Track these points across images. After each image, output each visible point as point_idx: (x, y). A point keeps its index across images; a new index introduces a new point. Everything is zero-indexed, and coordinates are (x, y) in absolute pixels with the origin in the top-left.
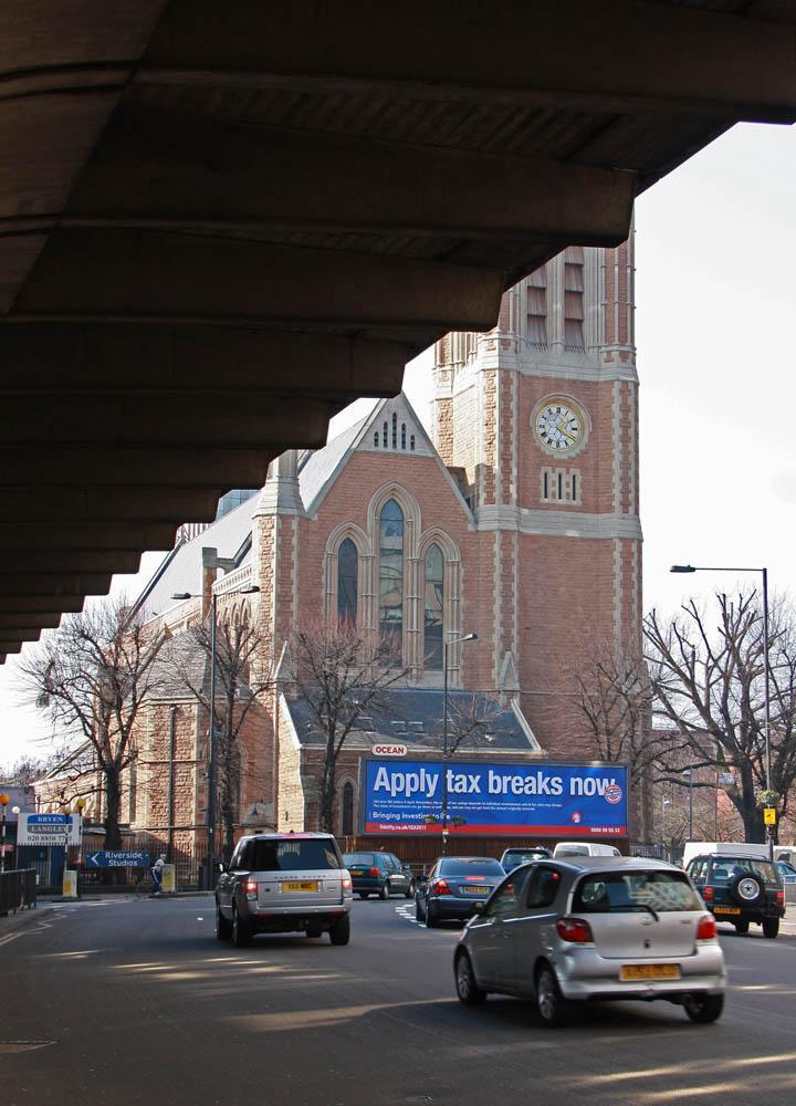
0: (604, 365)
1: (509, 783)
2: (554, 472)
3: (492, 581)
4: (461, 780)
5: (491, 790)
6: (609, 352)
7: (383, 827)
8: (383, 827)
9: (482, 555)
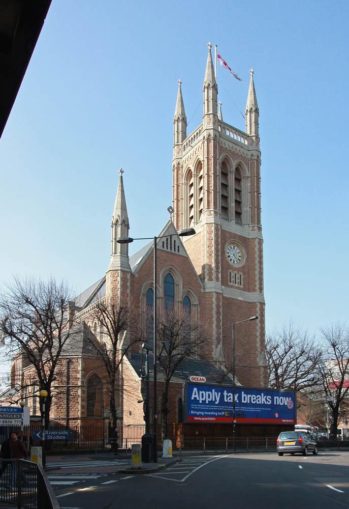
0: (251, 232)
1: (250, 398)
2: (238, 273)
3: (212, 314)
4: (230, 396)
5: (243, 401)
6: (253, 227)
7: (196, 418)
8: (196, 418)
9: (207, 303)
